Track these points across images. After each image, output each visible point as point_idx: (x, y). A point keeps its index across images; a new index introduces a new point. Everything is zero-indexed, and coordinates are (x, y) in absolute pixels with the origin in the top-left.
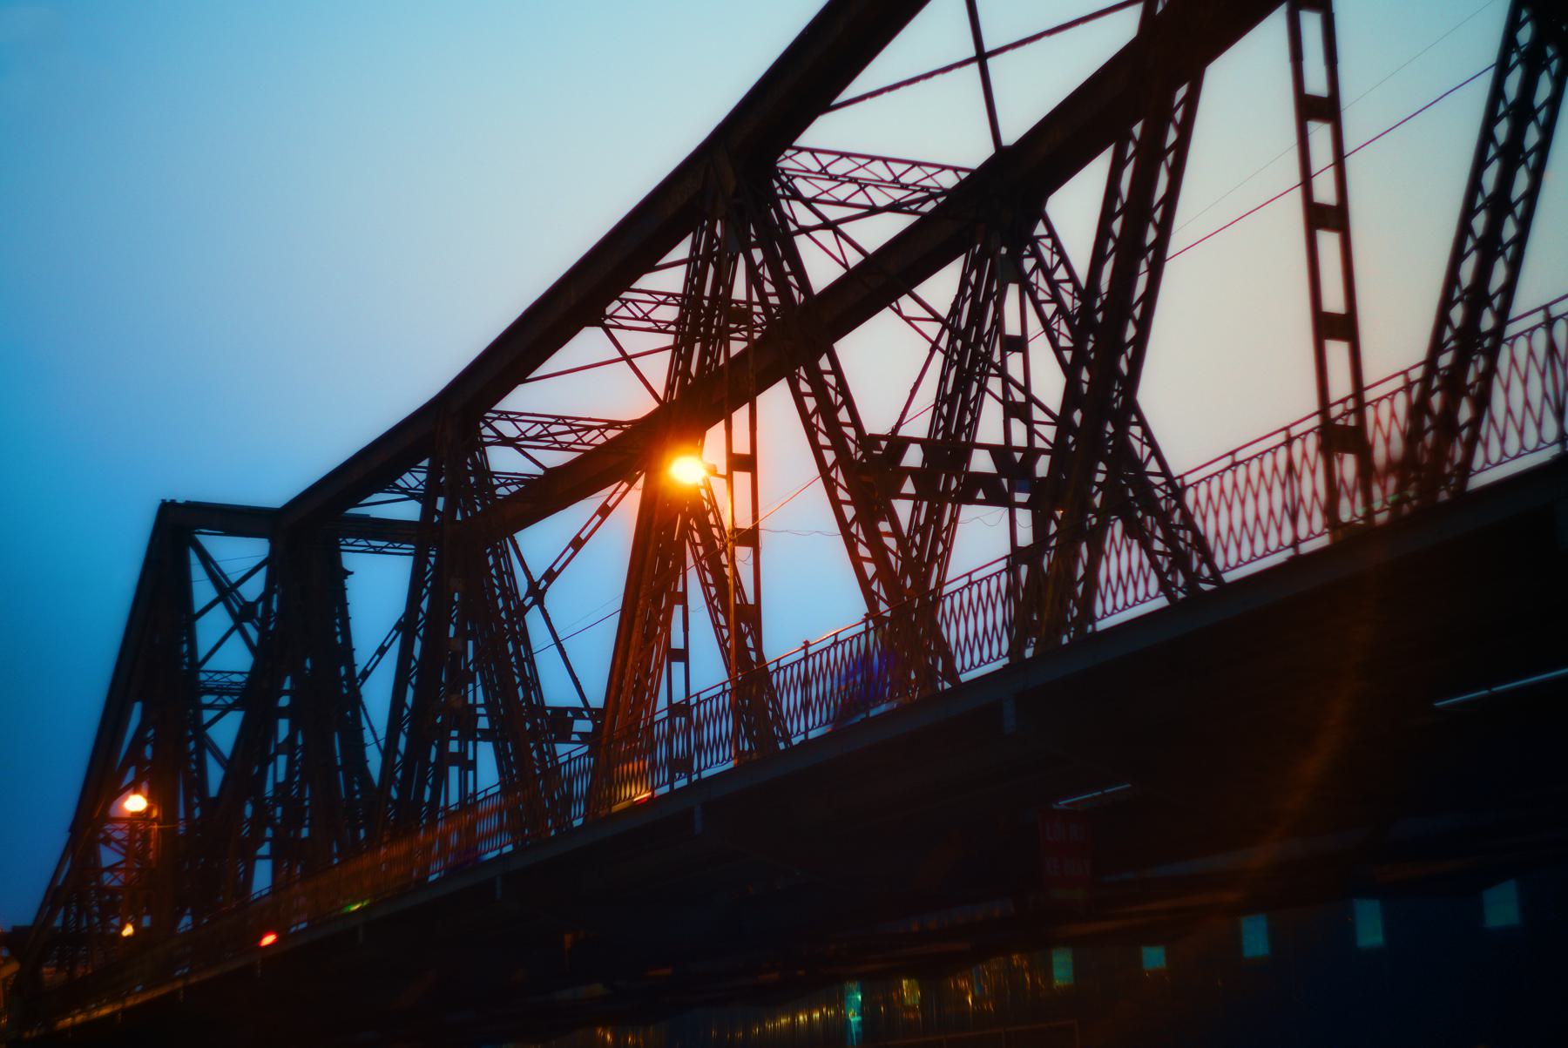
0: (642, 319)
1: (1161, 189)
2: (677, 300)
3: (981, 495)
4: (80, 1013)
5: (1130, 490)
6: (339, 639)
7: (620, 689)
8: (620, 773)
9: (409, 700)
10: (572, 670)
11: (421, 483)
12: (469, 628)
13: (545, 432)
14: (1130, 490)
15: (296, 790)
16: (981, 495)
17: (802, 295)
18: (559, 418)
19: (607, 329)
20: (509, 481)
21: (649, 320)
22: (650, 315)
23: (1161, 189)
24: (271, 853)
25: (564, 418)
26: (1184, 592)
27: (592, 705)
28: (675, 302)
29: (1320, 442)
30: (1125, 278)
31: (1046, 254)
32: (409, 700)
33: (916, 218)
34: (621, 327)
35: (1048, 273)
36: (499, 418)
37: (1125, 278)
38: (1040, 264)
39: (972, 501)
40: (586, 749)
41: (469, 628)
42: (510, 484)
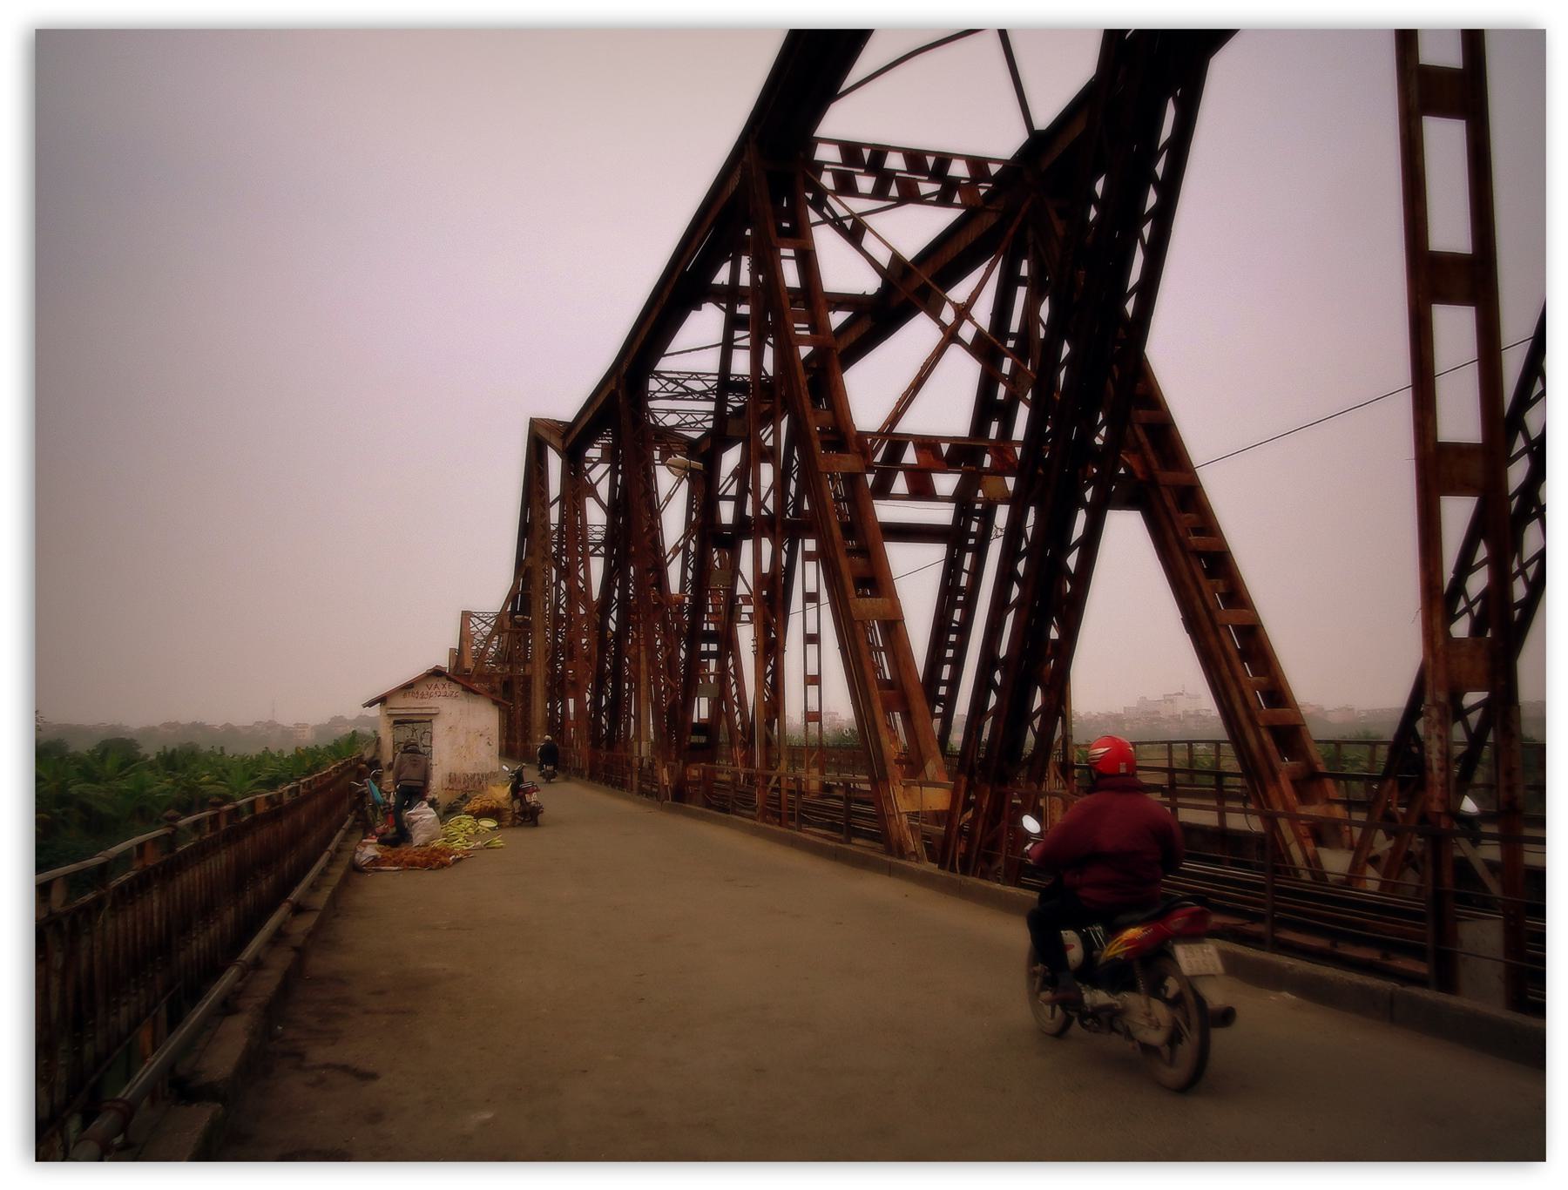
3: (945, 447)
5: (1091, 218)
6: (1130, 306)
7: (526, 608)
12: (785, 205)
13: (683, 422)
14: (1091, 218)
15: (564, 599)
16: (945, 447)
18: (693, 374)
20: (693, 425)
25: (696, 374)
26: (590, 460)
27: (654, 380)
29: (1540, 493)
36: (689, 379)
39: (955, 442)
40: (652, 404)
41: (785, 205)
42: (693, 423)
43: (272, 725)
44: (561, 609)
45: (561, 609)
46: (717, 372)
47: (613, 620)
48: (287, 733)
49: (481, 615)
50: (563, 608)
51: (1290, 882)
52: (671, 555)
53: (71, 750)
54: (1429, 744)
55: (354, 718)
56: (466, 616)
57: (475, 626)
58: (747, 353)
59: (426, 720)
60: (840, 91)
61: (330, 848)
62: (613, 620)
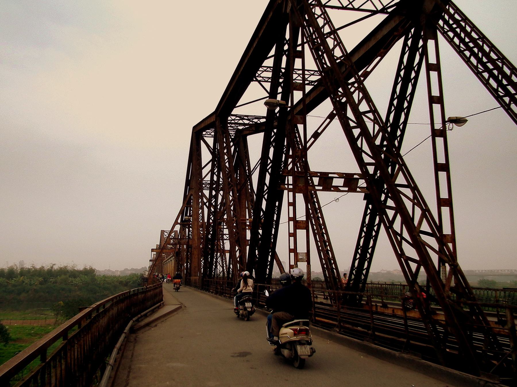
0: (209, 135)
1: (368, 218)
2: (318, 73)
4: (106, 358)
8: (73, 357)
9: (267, 181)
10: (322, 126)
11: (228, 238)
16: (339, 117)
17: (359, 146)
19: (259, 82)
21: (211, 135)
22: (308, 79)
23: (368, 218)
24: (122, 333)
28: (318, 74)
30: (397, 117)
31: (366, 148)
32: (267, 181)
33: (313, 86)
34: (206, 137)
35: (365, 132)
37: (397, 117)
38: (370, 141)
43: (109, 270)
44: (211, 220)
45: (211, 220)
46: (265, 115)
47: (249, 122)
48: (113, 272)
49: (168, 232)
50: (212, 220)
51: (165, 269)
52: (313, 139)
53: (102, 275)
54: (140, 274)
55: (123, 270)
56: (163, 232)
57: (166, 235)
58: (282, 67)
59: (145, 272)
60: (268, 56)
61: (125, 331)
62: (249, 122)
